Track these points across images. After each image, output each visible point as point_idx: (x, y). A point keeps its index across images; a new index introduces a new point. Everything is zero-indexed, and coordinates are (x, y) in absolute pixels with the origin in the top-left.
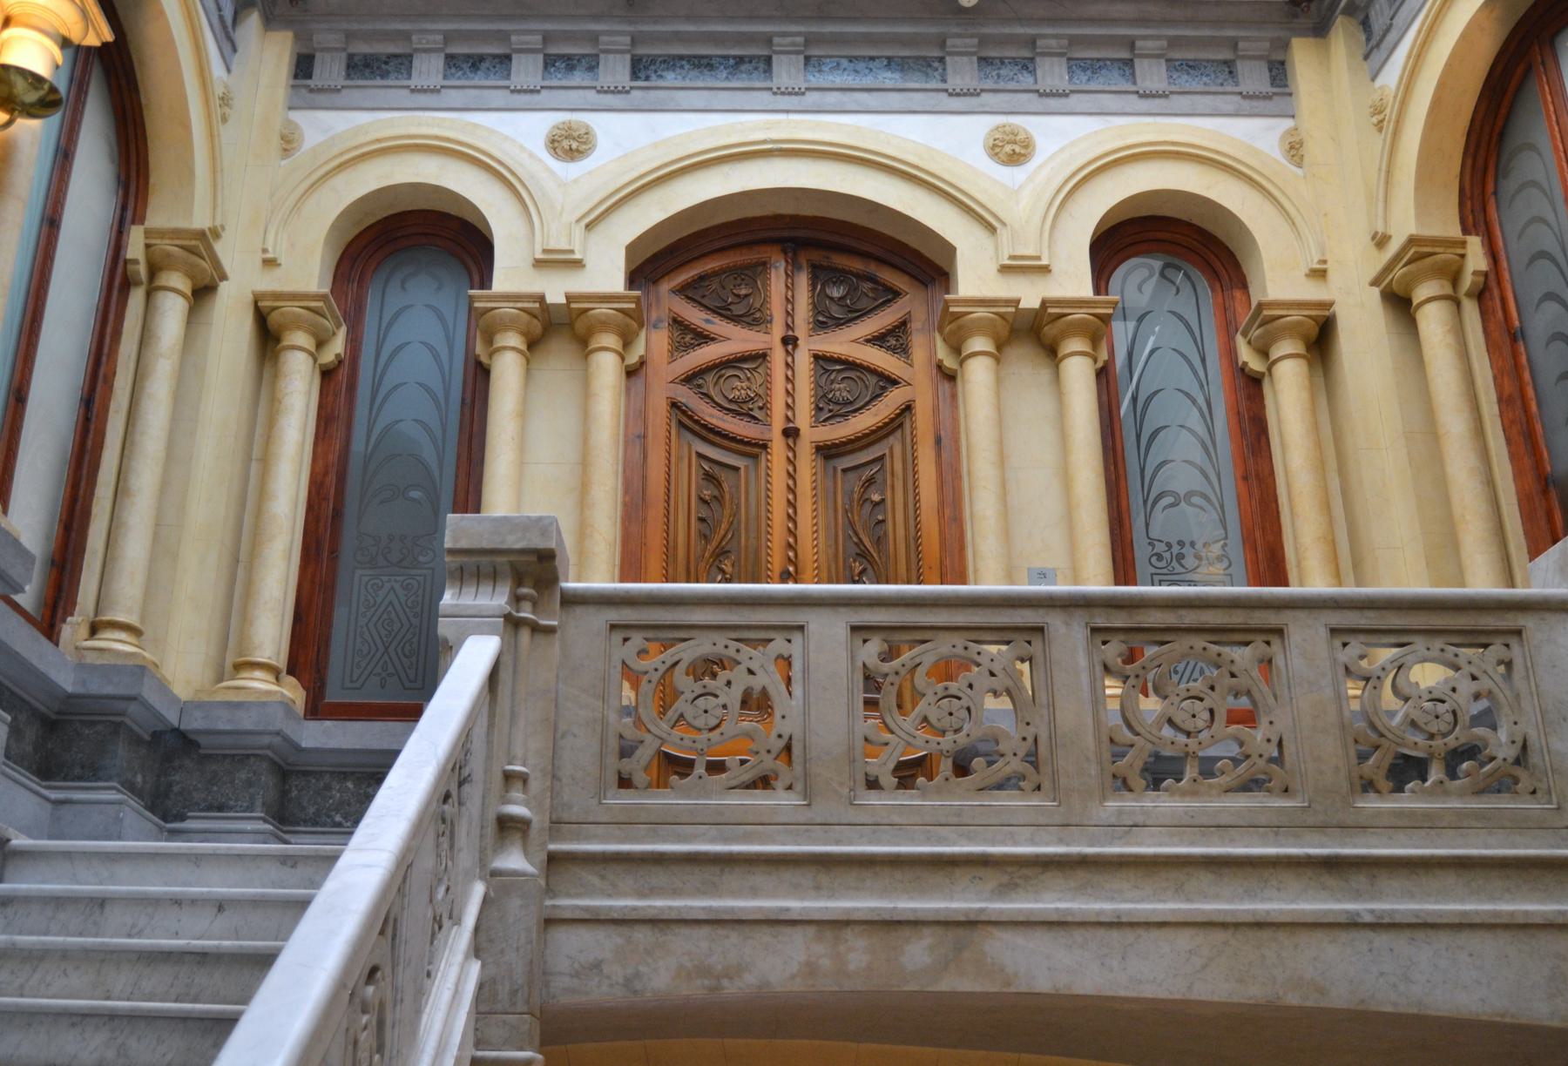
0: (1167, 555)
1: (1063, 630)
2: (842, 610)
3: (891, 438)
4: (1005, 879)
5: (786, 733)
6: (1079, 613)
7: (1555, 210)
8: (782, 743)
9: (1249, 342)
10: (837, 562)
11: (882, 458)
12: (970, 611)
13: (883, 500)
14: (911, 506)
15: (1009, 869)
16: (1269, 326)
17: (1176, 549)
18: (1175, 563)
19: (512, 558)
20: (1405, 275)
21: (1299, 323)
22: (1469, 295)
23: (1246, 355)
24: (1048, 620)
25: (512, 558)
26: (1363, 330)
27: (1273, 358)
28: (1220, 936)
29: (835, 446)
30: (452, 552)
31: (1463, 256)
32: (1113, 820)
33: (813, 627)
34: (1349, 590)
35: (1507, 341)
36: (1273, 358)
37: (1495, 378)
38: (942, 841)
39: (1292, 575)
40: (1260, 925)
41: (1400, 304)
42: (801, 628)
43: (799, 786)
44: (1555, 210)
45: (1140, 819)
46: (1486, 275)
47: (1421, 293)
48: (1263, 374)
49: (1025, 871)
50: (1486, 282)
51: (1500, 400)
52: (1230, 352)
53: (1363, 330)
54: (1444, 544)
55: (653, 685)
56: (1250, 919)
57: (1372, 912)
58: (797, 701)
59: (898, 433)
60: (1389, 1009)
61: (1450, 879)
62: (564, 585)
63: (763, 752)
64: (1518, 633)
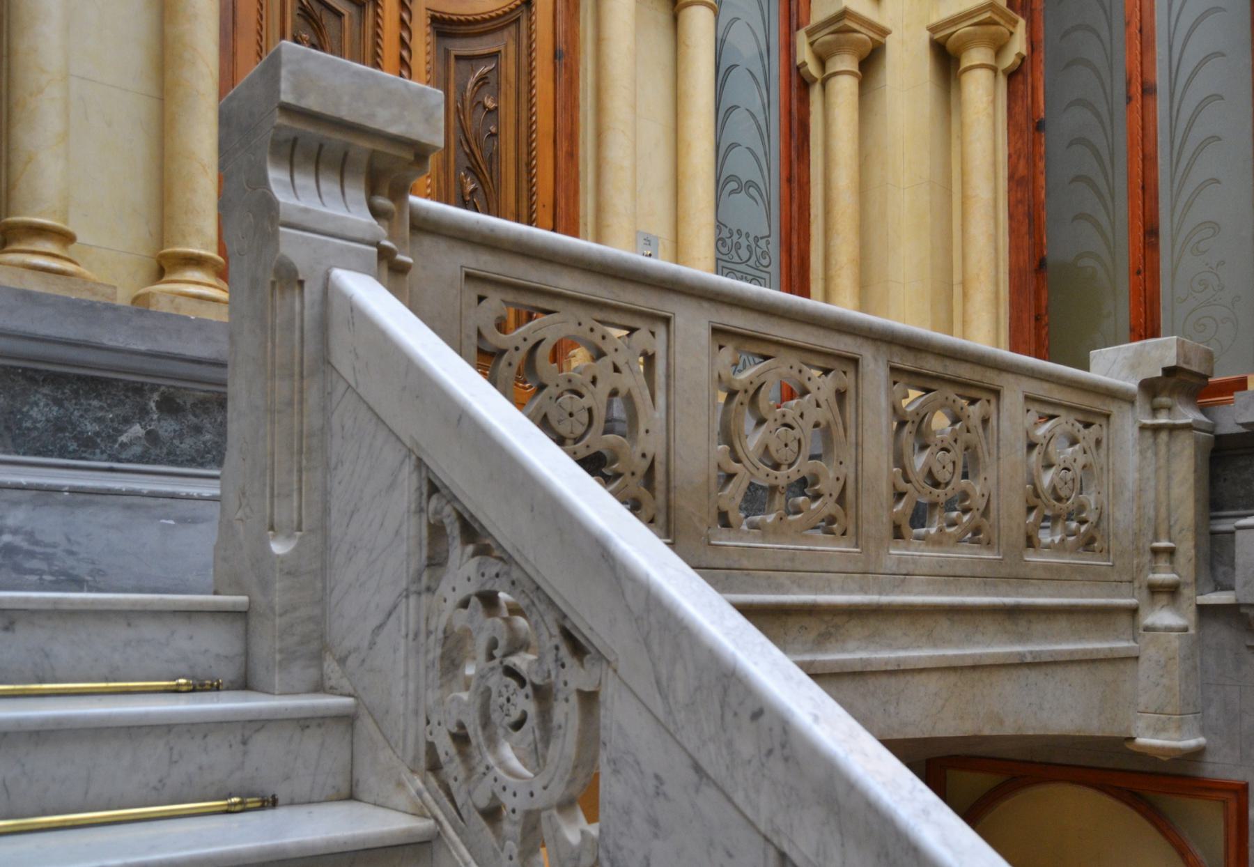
0: (729, 241)
1: (872, 366)
2: (706, 305)
3: (506, 33)
4: (823, 628)
5: (650, 451)
6: (884, 348)
7: (1110, 27)
8: (645, 464)
9: (812, 44)
10: (447, 173)
11: (494, 55)
12: (808, 329)
13: (496, 108)
14: (523, 128)
15: (827, 618)
16: (841, 36)
17: (735, 237)
18: (733, 252)
19: (380, 147)
20: (967, 34)
21: (865, 42)
22: (1004, 71)
23: (804, 54)
24: (862, 352)
25: (380, 147)
26: (907, 64)
27: (829, 71)
28: (952, 678)
29: (451, 22)
30: (286, 109)
31: (1012, 33)
32: (894, 569)
33: (679, 322)
34: (940, 337)
35: (1028, 128)
36: (829, 71)
37: (1010, 156)
38: (779, 589)
39: (816, 285)
40: (976, 667)
41: (946, 58)
42: (667, 321)
43: (661, 519)
44: (1110, 27)
45: (911, 568)
46: (1023, 59)
47: (977, 56)
48: (815, 80)
49: (837, 620)
50: (1020, 66)
51: (1011, 177)
52: (789, 48)
53: (907, 64)
54: (948, 289)
55: (514, 369)
56: (969, 662)
57: (1031, 652)
58: (660, 414)
59: (513, 29)
60: (1031, 733)
61: (1062, 623)
62: (413, 199)
63: (628, 474)
64: (1108, 416)
